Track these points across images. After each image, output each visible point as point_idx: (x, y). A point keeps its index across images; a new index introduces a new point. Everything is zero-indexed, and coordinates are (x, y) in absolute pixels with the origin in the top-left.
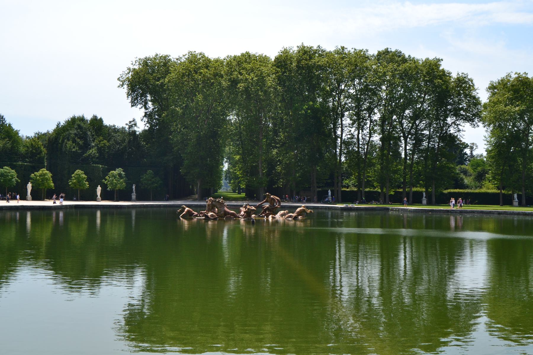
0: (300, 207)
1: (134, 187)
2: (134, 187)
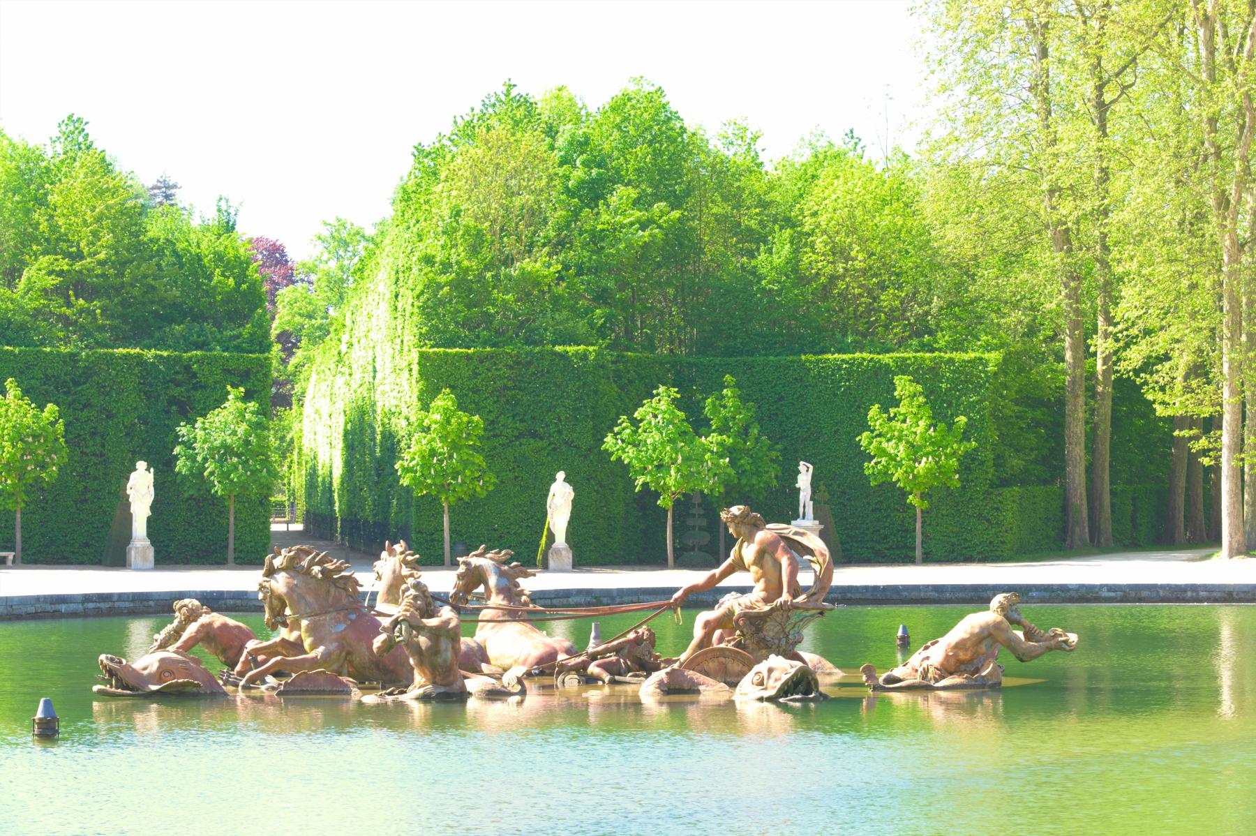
0: (978, 596)
1: (804, 480)
2: (804, 480)
